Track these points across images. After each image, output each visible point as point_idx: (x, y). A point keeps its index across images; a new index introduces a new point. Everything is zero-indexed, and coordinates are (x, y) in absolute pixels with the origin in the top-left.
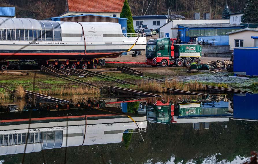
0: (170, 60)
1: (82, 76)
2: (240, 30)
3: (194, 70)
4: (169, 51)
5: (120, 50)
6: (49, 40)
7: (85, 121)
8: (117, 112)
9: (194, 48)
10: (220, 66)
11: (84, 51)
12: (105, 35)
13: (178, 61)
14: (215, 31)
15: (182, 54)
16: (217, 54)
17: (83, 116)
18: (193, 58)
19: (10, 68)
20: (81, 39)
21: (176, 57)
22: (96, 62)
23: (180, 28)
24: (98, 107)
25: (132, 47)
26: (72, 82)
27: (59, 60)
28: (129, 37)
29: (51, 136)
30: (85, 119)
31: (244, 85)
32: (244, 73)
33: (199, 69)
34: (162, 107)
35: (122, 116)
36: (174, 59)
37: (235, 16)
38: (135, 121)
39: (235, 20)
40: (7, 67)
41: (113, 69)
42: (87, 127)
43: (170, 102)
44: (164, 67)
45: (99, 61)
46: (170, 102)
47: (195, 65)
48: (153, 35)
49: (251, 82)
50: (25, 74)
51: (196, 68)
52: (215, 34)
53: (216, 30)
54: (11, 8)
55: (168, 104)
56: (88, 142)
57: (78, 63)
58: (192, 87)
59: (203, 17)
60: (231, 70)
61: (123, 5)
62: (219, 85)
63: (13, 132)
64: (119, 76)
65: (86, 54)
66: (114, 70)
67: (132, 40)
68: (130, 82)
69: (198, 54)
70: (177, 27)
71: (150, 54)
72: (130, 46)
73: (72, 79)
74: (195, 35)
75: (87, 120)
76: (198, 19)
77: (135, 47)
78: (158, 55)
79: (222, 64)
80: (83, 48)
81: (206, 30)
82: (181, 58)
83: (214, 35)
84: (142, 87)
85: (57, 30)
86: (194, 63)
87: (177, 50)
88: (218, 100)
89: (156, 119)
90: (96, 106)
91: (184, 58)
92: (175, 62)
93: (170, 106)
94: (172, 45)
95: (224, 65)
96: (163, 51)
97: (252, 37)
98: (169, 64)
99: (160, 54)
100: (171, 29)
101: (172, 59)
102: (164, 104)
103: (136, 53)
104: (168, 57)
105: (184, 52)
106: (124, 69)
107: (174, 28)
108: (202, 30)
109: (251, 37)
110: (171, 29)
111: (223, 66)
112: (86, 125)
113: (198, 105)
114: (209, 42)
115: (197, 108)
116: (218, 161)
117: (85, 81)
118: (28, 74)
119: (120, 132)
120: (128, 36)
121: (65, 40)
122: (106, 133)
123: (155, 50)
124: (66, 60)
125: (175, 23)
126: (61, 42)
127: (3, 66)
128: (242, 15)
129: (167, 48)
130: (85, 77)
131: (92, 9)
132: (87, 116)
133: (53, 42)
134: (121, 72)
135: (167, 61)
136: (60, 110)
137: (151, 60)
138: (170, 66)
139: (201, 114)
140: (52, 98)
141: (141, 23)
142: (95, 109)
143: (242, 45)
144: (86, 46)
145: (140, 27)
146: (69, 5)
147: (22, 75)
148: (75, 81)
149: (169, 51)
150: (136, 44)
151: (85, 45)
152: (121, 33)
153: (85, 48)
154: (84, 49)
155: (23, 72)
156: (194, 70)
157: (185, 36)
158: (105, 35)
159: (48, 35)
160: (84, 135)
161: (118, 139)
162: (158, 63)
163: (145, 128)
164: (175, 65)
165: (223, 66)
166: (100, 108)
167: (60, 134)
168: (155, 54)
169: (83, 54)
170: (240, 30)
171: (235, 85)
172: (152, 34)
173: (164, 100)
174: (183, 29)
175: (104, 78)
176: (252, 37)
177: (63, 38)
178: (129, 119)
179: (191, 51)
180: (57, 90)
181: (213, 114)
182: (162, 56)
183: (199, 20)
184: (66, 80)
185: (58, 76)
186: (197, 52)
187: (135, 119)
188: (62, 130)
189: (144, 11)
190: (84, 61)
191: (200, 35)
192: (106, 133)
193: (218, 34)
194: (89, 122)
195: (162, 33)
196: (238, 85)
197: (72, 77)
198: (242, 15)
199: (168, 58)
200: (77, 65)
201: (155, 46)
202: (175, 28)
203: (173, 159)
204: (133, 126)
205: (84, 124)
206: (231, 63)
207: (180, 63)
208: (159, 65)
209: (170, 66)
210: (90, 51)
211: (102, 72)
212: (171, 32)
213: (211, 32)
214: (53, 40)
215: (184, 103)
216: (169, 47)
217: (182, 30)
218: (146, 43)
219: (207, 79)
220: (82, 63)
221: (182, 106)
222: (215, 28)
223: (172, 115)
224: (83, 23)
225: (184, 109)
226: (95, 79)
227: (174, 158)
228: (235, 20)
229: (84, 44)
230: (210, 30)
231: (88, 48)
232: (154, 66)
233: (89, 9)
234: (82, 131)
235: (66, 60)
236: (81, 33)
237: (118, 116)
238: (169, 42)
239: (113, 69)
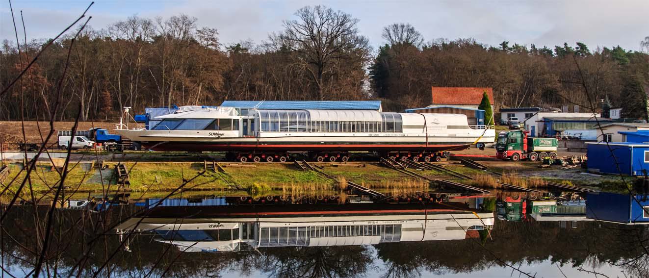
0: (522, 154)
1: (420, 168)
2: (608, 125)
3: (546, 166)
4: (522, 144)
5: (465, 143)
6: (391, 132)
7: (425, 215)
8: (462, 208)
9: (550, 142)
10: (576, 162)
11: (426, 143)
12: (449, 127)
13: (531, 156)
14: (583, 125)
15: (536, 148)
16: (582, 149)
17: (424, 211)
18: (548, 152)
19: (350, 160)
20: (423, 131)
21: (530, 150)
22: (439, 154)
23: (546, 121)
24: (441, 202)
25: (479, 139)
26: (406, 175)
27: (401, 152)
28: (475, 129)
29: (389, 229)
30: (425, 214)
31: (593, 183)
32: (598, 170)
33: (552, 164)
34: (513, 204)
35: (466, 211)
36: (527, 153)
37: (614, 110)
38: (480, 217)
39: (614, 114)
40: (348, 158)
41: (457, 162)
42: (427, 222)
43: (522, 199)
44: (515, 161)
45: (443, 153)
46: (522, 199)
47: (548, 160)
48: (521, 127)
49: (602, 179)
50: (362, 165)
51: (548, 164)
52: (583, 127)
53: (585, 124)
54: (377, 101)
55: (519, 201)
56: (429, 237)
57: (421, 156)
58: (532, 183)
59: (571, 110)
60: (584, 166)
61: (482, 97)
62: (563, 182)
63: (351, 224)
64: (460, 169)
65: (428, 146)
66: (458, 163)
67: (478, 132)
68: (469, 176)
69: (554, 149)
70: (543, 120)
71: (500, 147)
72: (476, 139)
73: (408, 172)
74: (561, 129)
75: (427, 215)
76: (565, 112)
77: (482, 140)
78: (509, 149)
79: (578, 160)
80: (424, 140)
81: (573, 123)
82: (536, 152)
83: (582, 129)
84: (476, 182)
85: (398, 121)
86: (547, 158)
87: (530, 143)
88: (573, 198)
89: (505, 216)
90: (439, 200)
91: (539, 152)
92: (528, 156)
93: (521, 203)
94: (525, 138)
95: (581, 160)
96: (515, 145)
97: (619, 133)
98: (521, 158)
99: (511, 148)
100: (536, 121)
101: (525, 153)
102: (514, 201)
103: (482, 146)
104: (521, 151)
105: (538, 146)
106: (469, 162)
107: (539, 120)
108: (568, 123)
109: (448, 126)
110: (536, 121)
111: (578, 162)
112: (426, 219)
113: (554, 203)
114: (576, 136)
115: (552, 206)
116: (552, 263)
117: (421, 174)
118: (364, 166)
119: (463, 228)
120: (474, 128)
121: (406, 131)
122: (448, 229)
123: (505, 143)
124: (407, 152)
125: (541, 115)
126: (402, 134)
127: (343, 158)
128: (621, 109)
129: (519, 141)
130: (423, 170)
131: (457, 101)
132: (427, 211)
133: (393, 134)
134: (464, 165)
135: (519, 155)
136: (400, 203)
137: (502, 154)
138: (523, 160)
139: (556, 212)
140: (371, 191)
141: (513, 115)
142: (438, 204)
143: (610, 140)
144: (428, 138)
145: (510, 119)
146: (434, 98)
147: (358, 167)
148: (410, 174)
149: (522, 144)
150: (483, 136)
151: (427, 137)
152: (467, 124)
153: (427, 140)
154: (425, 141)
155: (360, 163)
156: (546, 166)
157: (550, 129)
158: (449, 127)
159: (390, 127)
160: (423, 230)
161: (461, 235)
162: (509, 157)
163: (492, 226)
164: (528, 159)
165: (578, 162)
166: (444, 203)
167: (398, 228)
168: (506, 147)
169: (424, 146)
170: (608, 125)
171: (584, 182)
172: (519, 126)
173: (533, 196)
174: (549, 122)
175: (441, 171)
176: (619, 133)
177: (404, 130)
178: (473, 215)
179: (546, 145)
180: (383, 182)
181: (580, 212)
182: (514, 149)
183: (567, 113)
184: (400, 173)
185: (395, 169)
186: (553, 146)
187: (480, 215)
188: (399, 223)
189: (518, 103)
190: (425, 153)
191: (567, 128)
192: (448, 229)
193: (586, 127)
194: (429, 216)
195: (528, 126)
196: (586, 183)
197: (410, 170)
198: (621, 109)
199: (520, 152)
200: (397, 158)
201: (506, 139)
202: (541, 121)
203: (551, 257)
204: (478, 223)
205: (425, 218)
206: (586, 158)
207: (533, 158)
208: (510, 159)
209: (523, 160)
210: (432, 143)
211: (443, 166)
212: (536, 125)
213: (579, 126)
214: (393, 132)
215: (538, 200)
216: (522, 141)
217: (548, 123)
218: (494, 136)
219: (555, 176)
220: (424, 155)
221: (535, 204)
222: (583, 122)
223: (523, 212)
224: (425, 114)
225: (537, 206)
226: (433, 172)
227: (552, 257)
228: (614, 114)
229: (426, 136)
230: (578, 123)
231: (430, 140)
232: (505, 160)
233: (453, 101)
234: (422, 225)
235: (407, 152)
236: (423, 124)
237: (460, 211)
238: (522, 136)
239: (457, 162)
